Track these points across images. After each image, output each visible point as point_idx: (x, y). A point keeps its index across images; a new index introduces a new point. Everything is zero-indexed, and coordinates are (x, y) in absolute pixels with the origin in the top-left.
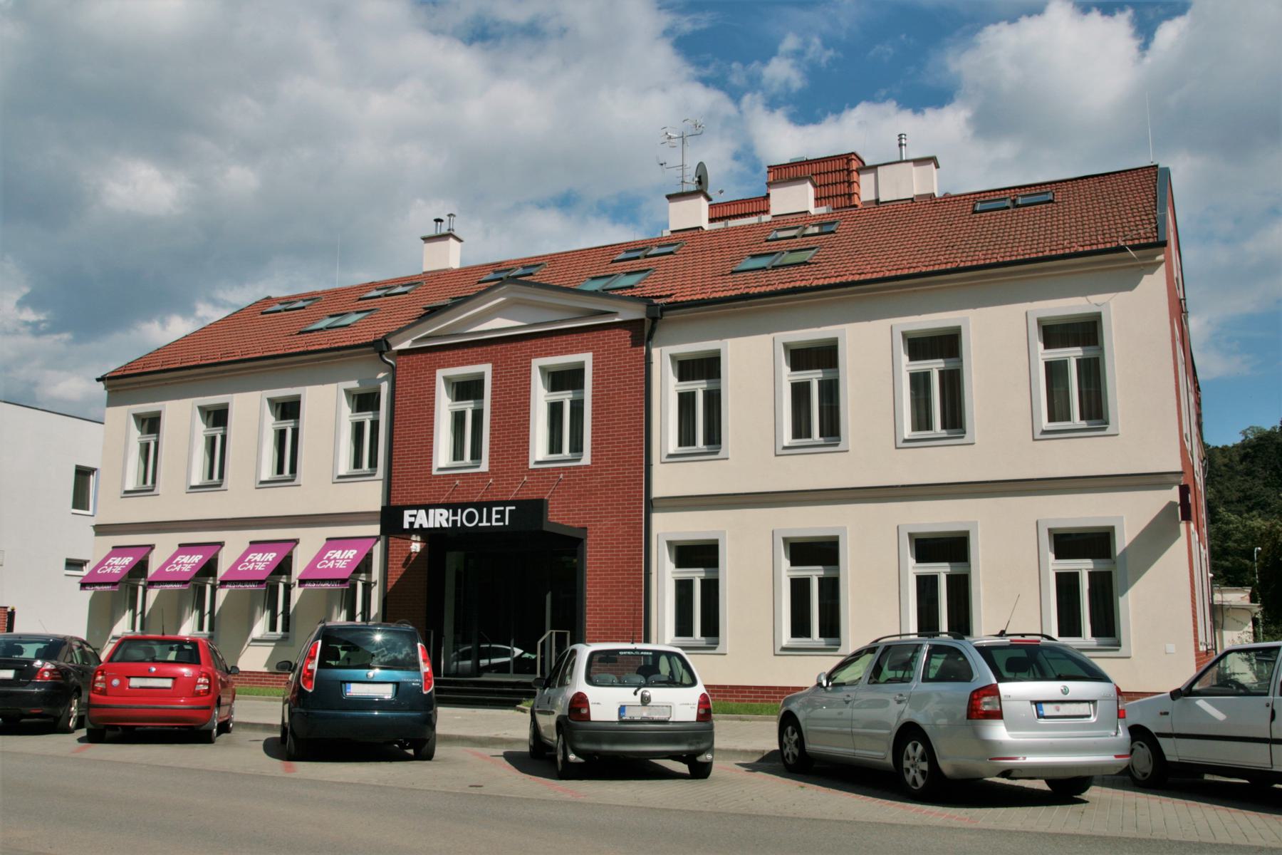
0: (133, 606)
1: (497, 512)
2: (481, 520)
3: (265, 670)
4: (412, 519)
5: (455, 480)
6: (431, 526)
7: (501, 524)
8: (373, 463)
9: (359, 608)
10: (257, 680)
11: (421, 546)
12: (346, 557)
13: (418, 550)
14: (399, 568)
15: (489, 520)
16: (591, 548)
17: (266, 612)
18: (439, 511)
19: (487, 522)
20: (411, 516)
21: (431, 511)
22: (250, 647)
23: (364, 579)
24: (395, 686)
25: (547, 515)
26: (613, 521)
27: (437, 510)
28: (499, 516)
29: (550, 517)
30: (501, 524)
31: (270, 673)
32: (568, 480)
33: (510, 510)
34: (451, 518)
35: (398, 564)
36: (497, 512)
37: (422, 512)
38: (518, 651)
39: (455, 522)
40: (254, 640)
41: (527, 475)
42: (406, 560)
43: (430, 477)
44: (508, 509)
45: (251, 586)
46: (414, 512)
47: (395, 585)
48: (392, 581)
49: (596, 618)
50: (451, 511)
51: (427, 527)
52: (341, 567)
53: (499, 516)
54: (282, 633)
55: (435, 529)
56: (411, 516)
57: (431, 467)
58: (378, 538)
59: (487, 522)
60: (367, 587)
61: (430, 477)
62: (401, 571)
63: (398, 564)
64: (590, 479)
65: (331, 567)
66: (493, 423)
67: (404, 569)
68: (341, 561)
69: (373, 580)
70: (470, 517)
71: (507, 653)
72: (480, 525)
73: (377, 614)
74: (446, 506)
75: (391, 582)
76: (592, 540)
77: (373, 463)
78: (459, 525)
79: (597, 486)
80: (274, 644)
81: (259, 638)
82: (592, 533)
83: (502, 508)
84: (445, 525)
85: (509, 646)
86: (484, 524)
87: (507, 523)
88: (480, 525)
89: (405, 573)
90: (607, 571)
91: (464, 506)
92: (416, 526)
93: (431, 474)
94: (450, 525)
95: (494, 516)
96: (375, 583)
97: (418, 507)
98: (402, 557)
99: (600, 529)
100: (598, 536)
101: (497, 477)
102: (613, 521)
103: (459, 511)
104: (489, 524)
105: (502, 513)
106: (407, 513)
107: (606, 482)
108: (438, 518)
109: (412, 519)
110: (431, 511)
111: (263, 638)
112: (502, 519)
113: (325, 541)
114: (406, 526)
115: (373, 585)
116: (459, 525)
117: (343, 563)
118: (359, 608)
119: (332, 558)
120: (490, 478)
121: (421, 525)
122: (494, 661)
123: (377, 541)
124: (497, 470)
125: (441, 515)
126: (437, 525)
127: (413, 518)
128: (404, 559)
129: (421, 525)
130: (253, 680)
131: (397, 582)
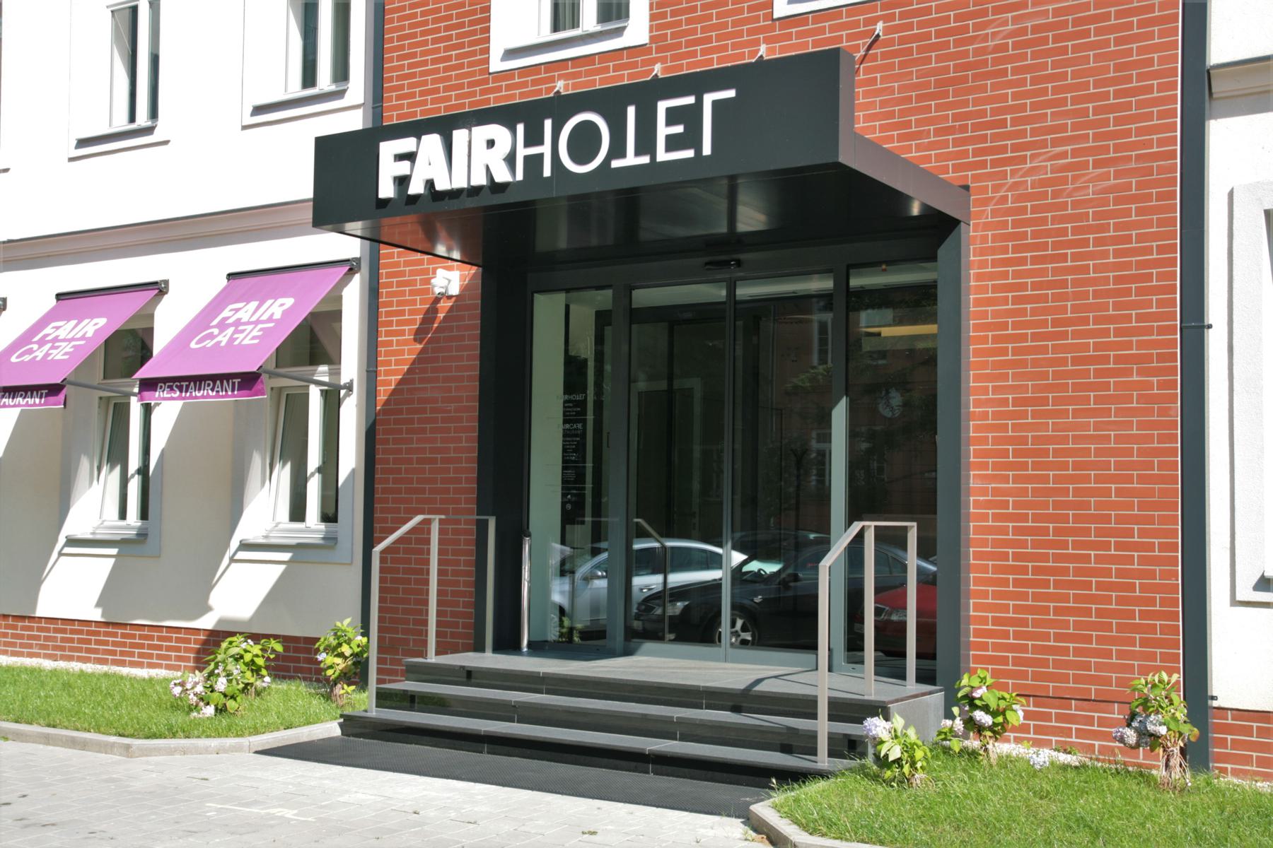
0: (116, 453)
1: (674, 116)
2: (618, 149)
3: (96, 615)
4: (403, 168)
5: (552, 80)
6: (460, 182)
7: (689, 154)
8: (341, 72)
9: (314, 458)
10: (80, 641)
11: (462, 278)
12: (264, 318)
13: (455, 290)
14: (405, 343)
15: (646, 143)
16: (982, 252)
17: (277, 467)
18: (482, 132)
19: (638, 153)
20: (400, 157)
21: (459, 136)
22: (62, 558)
23: (326, 379)
24: (851, 271)
25: (852, 120)
26: (1064, 155)
27: (476, 130)
28: (679, 129)
29: (859, 126)
30: (689, 154)
31: (107, 624)
32: (903, 40)
33: (716, 104)
34: (522, 152)
35: (402, 333)
36: (674, 116)
37: (432, 142)
38: (738, 557)
39: (534, 163)
40: (72, 542)
41: (767, 41)
42: (424, 321)
43: (486, 81)
44: (709, 99)
45: (31, 401)
46: (407, 144)
47: (394, 392)
48: (389, 380)
49: (1005, 479)
50: (520, 128)
51: (448, 187)
52: (247, 342)
53: (679, 129)
54: (139, 524)
55: (474, 191)
56: (400, 157)
57: (487, 51)
58: (351, 267)
59: (638, 153)
60: (332, 400)
61: (486, 81)
62: (411, 351)
63: (402, 333)
64: (977, 27)
65: (223, 344)
66: (659, 27)
67: (419, 346)
68: (249, 328)
69: (344, 380)
70: (584, 143)
71: (712, 562)
72: (616, 164)
73: (353, 471)
74: (505, 116)
75: (388, 383)
76: (987, 226)
77: (341, 72)
78: (547, 172)
79: (1004, 48)
80: (114, 551)
81: (90, 537)
82: (986, 202)
83: (690, 100)
84: (502, 175)
85: (720, 546)
86: (631, 159)
87: (707, 150)
88: (616, 164)
89: (420, 360)
90: (1044, 324)
91: (561, 108)
92: (416, 188)
93: (487, 70)
94: (520, 176)
95: (663, 131)
96: (349, 387)
97: (417, 129)
98: (411, 312)
99: (1015, 186)
100: (1009, 212)
101: (674, 58)
102: (1064, 155)
103: (548, 124)
104: (645, 160)
105: (689, 117)
106: (388, 149)
107: (1036, 29)
108: (482, 156)
109: (403, 168)
110: (459, 136)
111: (98, 537)
112: (691, 138)
113: (224, 282)
114: (386, 190)
115: (343, 392)
116: (547, 172)
117: (255, 333)
118: (314, 458)
119: (230, 321)
120: (654, 61)
121: (430, 184)
122: (678, 578)
123: (352, 271)
124: (674, 35)
125: (491, 144)
126: (479, 179)
127: (407, 164)
128: (419, 317)
129: (430, 184)
130: (72, 640)
131: (400, 382)
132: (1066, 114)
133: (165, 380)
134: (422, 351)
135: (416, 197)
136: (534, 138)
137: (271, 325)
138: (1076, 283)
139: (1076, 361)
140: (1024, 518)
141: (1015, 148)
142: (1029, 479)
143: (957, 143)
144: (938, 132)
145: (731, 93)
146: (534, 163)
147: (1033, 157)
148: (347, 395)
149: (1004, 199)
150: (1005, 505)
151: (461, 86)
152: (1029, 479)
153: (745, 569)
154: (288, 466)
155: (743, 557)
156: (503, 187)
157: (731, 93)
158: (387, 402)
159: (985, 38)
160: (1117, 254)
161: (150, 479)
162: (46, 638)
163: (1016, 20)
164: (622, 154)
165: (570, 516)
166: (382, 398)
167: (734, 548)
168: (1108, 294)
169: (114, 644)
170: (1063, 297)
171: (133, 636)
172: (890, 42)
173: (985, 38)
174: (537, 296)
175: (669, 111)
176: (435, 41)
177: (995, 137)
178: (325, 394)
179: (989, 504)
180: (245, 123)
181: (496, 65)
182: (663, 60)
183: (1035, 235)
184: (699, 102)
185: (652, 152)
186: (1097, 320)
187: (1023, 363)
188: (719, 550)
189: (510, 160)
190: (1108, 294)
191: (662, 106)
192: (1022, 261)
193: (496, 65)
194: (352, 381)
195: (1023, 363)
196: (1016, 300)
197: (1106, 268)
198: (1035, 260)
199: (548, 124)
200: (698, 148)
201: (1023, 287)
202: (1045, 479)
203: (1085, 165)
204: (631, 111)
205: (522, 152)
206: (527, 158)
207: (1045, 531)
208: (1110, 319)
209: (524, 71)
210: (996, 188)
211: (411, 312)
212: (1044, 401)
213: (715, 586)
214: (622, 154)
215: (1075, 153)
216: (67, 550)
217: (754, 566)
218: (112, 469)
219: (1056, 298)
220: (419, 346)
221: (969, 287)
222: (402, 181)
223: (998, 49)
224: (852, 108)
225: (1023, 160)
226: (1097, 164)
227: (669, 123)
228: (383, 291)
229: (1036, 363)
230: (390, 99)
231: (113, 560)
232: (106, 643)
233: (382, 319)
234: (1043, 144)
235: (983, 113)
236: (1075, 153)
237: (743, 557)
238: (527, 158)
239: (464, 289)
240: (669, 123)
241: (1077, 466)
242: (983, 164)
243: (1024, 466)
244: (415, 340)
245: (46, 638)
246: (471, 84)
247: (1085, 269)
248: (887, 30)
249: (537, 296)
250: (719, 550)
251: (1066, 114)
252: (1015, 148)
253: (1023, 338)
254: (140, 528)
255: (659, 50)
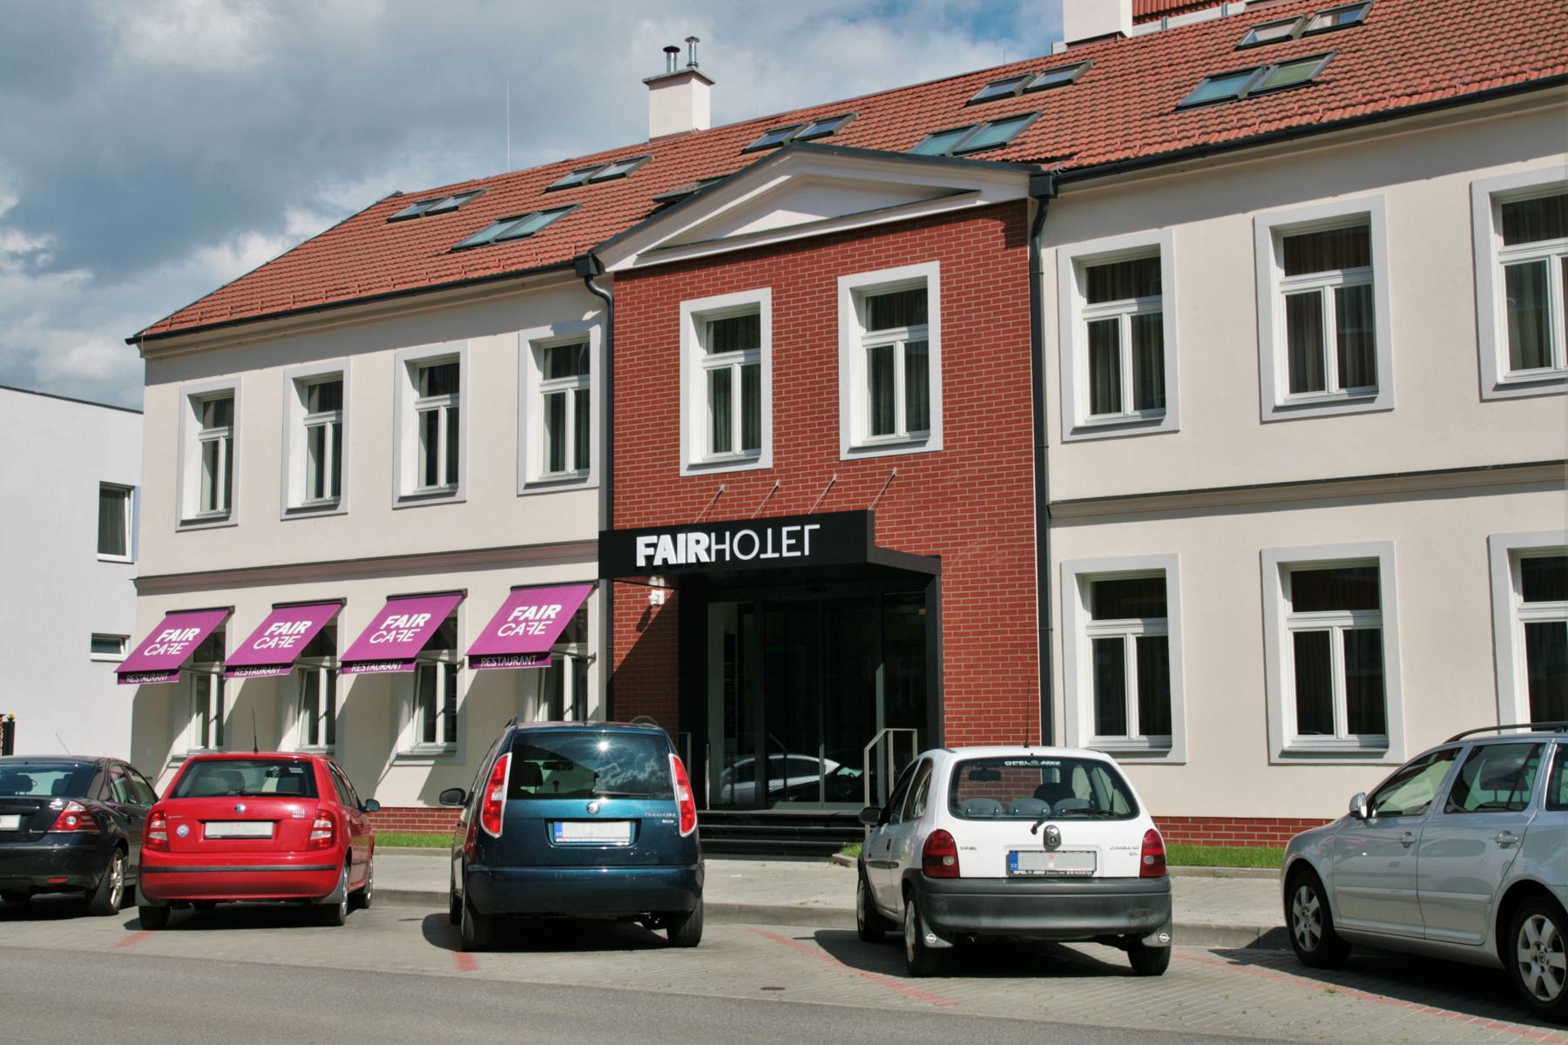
1: (790, 535)
2: (763, 549)
4: (651, 551)
5: (717, 483)
6: (682, 560)
7: (798, 554)
8: (582, 462)
9: (323, 708)
11: (666, 595)
13: (662, 602)
15: (777, 547)
18: (693, 536)
19: (774, 551)
20: (648, 546)
22: (393, 768)
23: (575, 652)
25: (874, 538)
26: (984, 542)
28: (793, 541)
29: (877, 540)
30: (798, 554)
33: (811, 531)
34: (714, 547)
36: (790, 535)
37: (666, 539)
38: (831, 765)
39: (720, 553)
40: (400, 757)
41: (837, 472)
42: (642, 619)
43: (678, 481)
44: (807, 528)
48: (621, 654)
49: (961, 706)
50: (713, 535)
53: (793, 541)
55: (688, 565)
56: (648, 546)
58: (594, 585)
59: (774, 551)
60: (581, 664)
62: (635, 637)
63: (629, 626)
65: (521, 633)
67: (640, 634)
68: (536, 624)
69: (590, 653)
70: (746, 545)
71: (814, 769)
72: (762, 556)
73: (597, 708)
74: (705, 528)
75: (621, 655)
76: (950, 577)
77: (582, 462)
78: (728, 558)
80: (432, 762)
82: (949, 564)
83: (798, 528)
84: (704, 558)
85: (817, 756)
86: (770, 554)
87: (807, 552)
88: (762, 556)
91: (735, 527)
92: (658, 562)
94: (713, 559)
95: (785, 542)
96: (594, 658)
97: (658, 531)
98: (634, 614)
99: (962, 557)
100: (960, 570)
102: (984, 542)
103: (728, 534)
104: (777, 555)
105: (798, 536)
106: (641, 541)
109: (651, 551)
110: (681, 537)
112: (798, 546)
114: (641, 562)
115: (589, 661)
116: (728, 558)
118: (323, 708)
120: (776, 478)
121: (665, 560)
125: (698, 542)
126: (692, 560)
127: (652, 549)
128: (640, 617)
129: (665, 560)
131: (628, 655)
132: (985, 522)
133: (486, 656)
134: (642, 637)
135: (658, 567)
136: (720, 540)
137: (550, 622)
138: (992, 607)
139: (993, 646)
140: (970, 725)
141: (962, 537)
142: (972, 706)
143: (935, 533)
144: (925, 527)
145: (817, 526)
146: (720, 553)
147: (971, 542)
148: (591, 663)
149: (957, 563)
150: (961, 719)
151: (663, 483)
152: (972, 706)
153: (840, 773)
154: (308, 713)
155: (836, 765)
156: (705, 564)
157: (817, 526)
158: (620, 667)
159: (946, 481)
160: (1010, 593)
161: (337, 723)
162: (382, 821)
163: (961, 473)
164: (766, 552)
165: (729, 733)
166: (617, 664)
167: (827, 756)
168: (1007, 613)
169: (433, 822)
170: (987, 614)
171: (447, 816)
172: (900, 478)
173: (946, 481)
174: (710, 604)
175: (788, 533)
176: (645, 455)
177: (952, 532)
178: (574, 661)
179: (953, 719)
180: (520, 493)
181: (684, 472)
182: (781, 477)
183: (973, 582)
184: (803, 529)
185: (780, 551)
186: (1002, 626)
187: (968, 647)
188: (817, 760)
189: (708, 550)
190: (1007, 613)
191: (785, 530)
192: (967, 595)
193: (684, 472)
194: (595, 654)
195: (968, 647)
196: (964, 615)
197: (1005, 600)
198: (973, 595)
199: (728, 534)
200: (803, 552)
201: (967, 608)
202: (980, 705)
203: (994, 548)
204: (770, 531)
205: (714, 547)
206: (717, 551)
207: (980, 732)
208: (1008, 625)
209: (701, 477)
210: (953, 557)
211: (634, 614)
212: (978, 666)
213: (816, 784)
214: (766, 552)
215: (990, 542)
216: (396, 763)
217: (846, 771)
218: (198, 715)
219: (983, 614)
220: (640, 634)
221: (941, 608)
222: (650, 559)
223: (952, 486)
224: (873, 531)
225: (966, 544)
226: (1000, 548)
227: (789, 538)
228: (616, 600)
229: (974, 647)
230: (618, 487)
231: (430, 768)
232: (427, 821)
233: (616, 617)
234: (975, 536)
235: (946, 519)
236: (990, 542)
237: (836, 765)
238: (717, 551)
239: (667, 601)
240: (789, 538)
241: (994, 699)
242: (947, 545)
243: (969, 699)
244: (637, 630)
245: (382, 821)
246: (669, 482)
247: (996, 600)
248: (899, 472)
249: (710, 604)
250: (817, 760)
251: (985, 522)
252: (962, 537)
253: (968, 634)
254: (446, 747)
255: (778, 472)
